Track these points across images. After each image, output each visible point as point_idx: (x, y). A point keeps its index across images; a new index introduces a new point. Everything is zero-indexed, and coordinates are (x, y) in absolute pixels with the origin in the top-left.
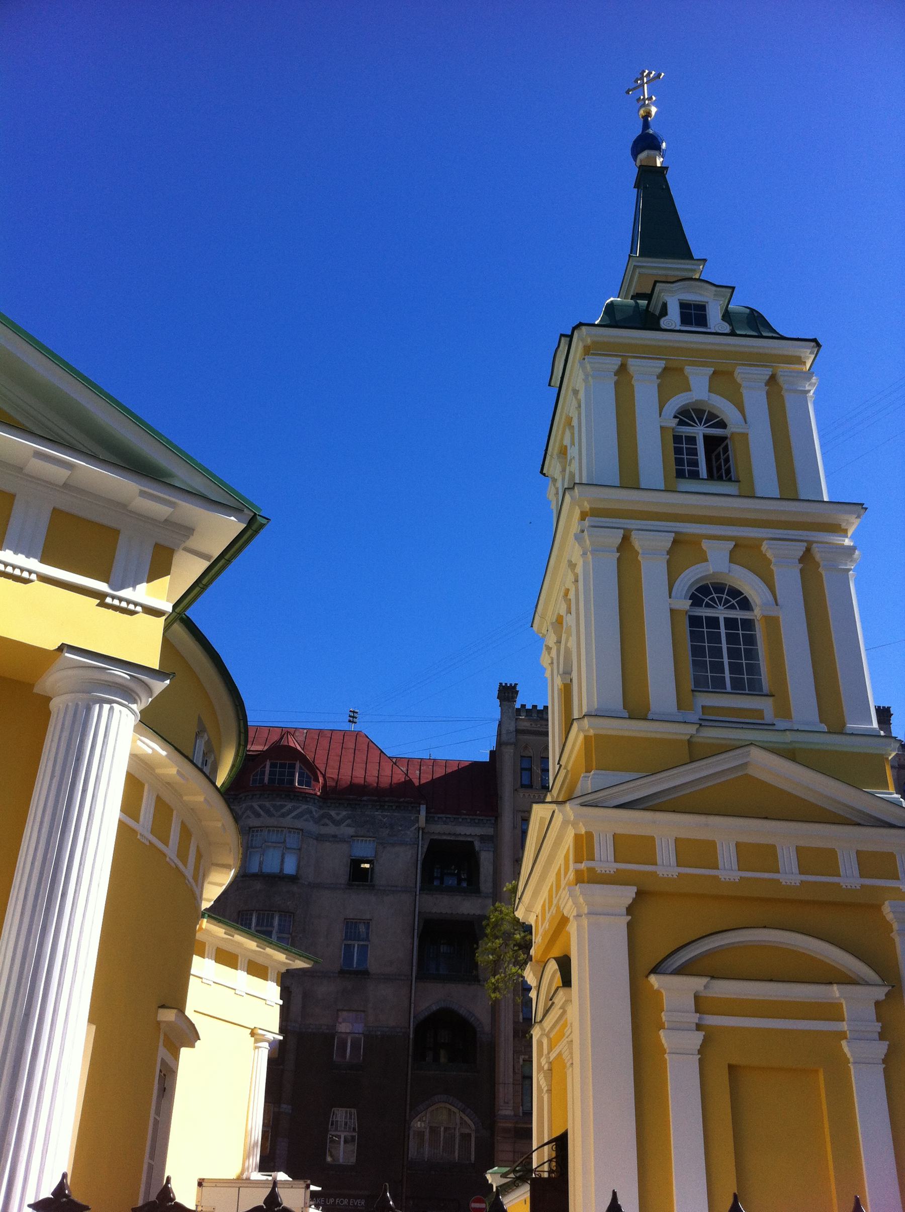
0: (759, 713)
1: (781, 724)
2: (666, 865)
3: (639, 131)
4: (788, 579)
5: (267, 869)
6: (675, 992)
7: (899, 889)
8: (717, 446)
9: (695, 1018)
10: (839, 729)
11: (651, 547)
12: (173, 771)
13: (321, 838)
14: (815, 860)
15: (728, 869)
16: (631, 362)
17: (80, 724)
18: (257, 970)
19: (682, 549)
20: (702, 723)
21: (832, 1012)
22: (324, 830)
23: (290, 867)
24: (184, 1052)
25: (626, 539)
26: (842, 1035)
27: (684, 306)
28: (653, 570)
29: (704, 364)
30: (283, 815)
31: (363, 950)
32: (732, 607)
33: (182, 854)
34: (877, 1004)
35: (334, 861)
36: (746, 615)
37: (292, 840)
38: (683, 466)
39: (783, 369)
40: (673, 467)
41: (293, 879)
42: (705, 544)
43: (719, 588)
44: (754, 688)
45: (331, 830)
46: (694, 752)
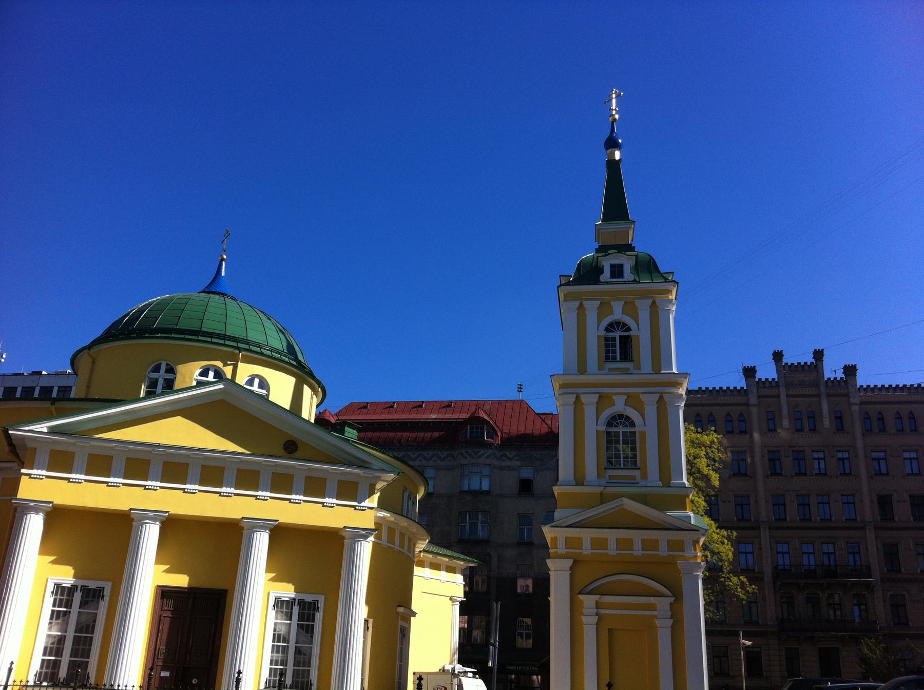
0: (634, 477)
1: (643, 483)
2: (587, 550)
3: (608, 134)
4: (651, 412)
5: (472, 488)
6: (589, 601)
7: (684, 556)
8: (626, 342)
9: (595, 611)
10: (667, 485)
11: (589, 401)
12: (392, 519)
13: (502, 468)
14: (648, 545)
15: (612, 550)
16: (584, 302)
17: (352, 550)
18: (451, 570)
19: (603, 400)
20: (609, 484)
21: (652, 607)
22: (504, 464)
23: (485, 486)
24: (412, 618)
25: (578, 398)
26: (656, 617)
27: (612, 266)
28: (590, 412)
29: (620, 300)
30: (480, 457)
31: (530, 530)
32: (626, 426)
33: (402, 546)
34: (671, 604)
35: (510, 482)
36: (632, 430)
37: (486, 471)
38: (609, 357)
39: (659, 298)
40: (603, 354)
41: (487, 493)
42: (614, 397)
43: (621, 416)
44: (635, 467)
45: (507, 463)
46: (603, 499)
